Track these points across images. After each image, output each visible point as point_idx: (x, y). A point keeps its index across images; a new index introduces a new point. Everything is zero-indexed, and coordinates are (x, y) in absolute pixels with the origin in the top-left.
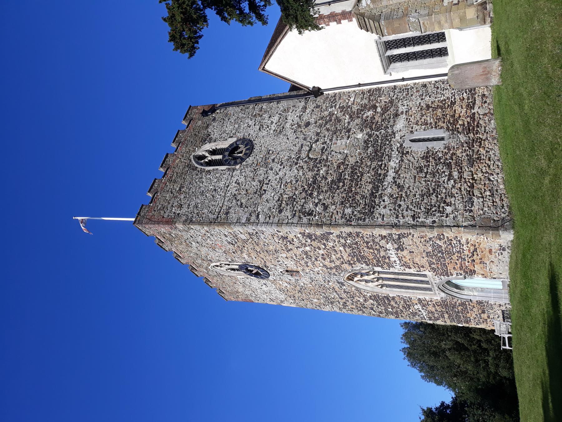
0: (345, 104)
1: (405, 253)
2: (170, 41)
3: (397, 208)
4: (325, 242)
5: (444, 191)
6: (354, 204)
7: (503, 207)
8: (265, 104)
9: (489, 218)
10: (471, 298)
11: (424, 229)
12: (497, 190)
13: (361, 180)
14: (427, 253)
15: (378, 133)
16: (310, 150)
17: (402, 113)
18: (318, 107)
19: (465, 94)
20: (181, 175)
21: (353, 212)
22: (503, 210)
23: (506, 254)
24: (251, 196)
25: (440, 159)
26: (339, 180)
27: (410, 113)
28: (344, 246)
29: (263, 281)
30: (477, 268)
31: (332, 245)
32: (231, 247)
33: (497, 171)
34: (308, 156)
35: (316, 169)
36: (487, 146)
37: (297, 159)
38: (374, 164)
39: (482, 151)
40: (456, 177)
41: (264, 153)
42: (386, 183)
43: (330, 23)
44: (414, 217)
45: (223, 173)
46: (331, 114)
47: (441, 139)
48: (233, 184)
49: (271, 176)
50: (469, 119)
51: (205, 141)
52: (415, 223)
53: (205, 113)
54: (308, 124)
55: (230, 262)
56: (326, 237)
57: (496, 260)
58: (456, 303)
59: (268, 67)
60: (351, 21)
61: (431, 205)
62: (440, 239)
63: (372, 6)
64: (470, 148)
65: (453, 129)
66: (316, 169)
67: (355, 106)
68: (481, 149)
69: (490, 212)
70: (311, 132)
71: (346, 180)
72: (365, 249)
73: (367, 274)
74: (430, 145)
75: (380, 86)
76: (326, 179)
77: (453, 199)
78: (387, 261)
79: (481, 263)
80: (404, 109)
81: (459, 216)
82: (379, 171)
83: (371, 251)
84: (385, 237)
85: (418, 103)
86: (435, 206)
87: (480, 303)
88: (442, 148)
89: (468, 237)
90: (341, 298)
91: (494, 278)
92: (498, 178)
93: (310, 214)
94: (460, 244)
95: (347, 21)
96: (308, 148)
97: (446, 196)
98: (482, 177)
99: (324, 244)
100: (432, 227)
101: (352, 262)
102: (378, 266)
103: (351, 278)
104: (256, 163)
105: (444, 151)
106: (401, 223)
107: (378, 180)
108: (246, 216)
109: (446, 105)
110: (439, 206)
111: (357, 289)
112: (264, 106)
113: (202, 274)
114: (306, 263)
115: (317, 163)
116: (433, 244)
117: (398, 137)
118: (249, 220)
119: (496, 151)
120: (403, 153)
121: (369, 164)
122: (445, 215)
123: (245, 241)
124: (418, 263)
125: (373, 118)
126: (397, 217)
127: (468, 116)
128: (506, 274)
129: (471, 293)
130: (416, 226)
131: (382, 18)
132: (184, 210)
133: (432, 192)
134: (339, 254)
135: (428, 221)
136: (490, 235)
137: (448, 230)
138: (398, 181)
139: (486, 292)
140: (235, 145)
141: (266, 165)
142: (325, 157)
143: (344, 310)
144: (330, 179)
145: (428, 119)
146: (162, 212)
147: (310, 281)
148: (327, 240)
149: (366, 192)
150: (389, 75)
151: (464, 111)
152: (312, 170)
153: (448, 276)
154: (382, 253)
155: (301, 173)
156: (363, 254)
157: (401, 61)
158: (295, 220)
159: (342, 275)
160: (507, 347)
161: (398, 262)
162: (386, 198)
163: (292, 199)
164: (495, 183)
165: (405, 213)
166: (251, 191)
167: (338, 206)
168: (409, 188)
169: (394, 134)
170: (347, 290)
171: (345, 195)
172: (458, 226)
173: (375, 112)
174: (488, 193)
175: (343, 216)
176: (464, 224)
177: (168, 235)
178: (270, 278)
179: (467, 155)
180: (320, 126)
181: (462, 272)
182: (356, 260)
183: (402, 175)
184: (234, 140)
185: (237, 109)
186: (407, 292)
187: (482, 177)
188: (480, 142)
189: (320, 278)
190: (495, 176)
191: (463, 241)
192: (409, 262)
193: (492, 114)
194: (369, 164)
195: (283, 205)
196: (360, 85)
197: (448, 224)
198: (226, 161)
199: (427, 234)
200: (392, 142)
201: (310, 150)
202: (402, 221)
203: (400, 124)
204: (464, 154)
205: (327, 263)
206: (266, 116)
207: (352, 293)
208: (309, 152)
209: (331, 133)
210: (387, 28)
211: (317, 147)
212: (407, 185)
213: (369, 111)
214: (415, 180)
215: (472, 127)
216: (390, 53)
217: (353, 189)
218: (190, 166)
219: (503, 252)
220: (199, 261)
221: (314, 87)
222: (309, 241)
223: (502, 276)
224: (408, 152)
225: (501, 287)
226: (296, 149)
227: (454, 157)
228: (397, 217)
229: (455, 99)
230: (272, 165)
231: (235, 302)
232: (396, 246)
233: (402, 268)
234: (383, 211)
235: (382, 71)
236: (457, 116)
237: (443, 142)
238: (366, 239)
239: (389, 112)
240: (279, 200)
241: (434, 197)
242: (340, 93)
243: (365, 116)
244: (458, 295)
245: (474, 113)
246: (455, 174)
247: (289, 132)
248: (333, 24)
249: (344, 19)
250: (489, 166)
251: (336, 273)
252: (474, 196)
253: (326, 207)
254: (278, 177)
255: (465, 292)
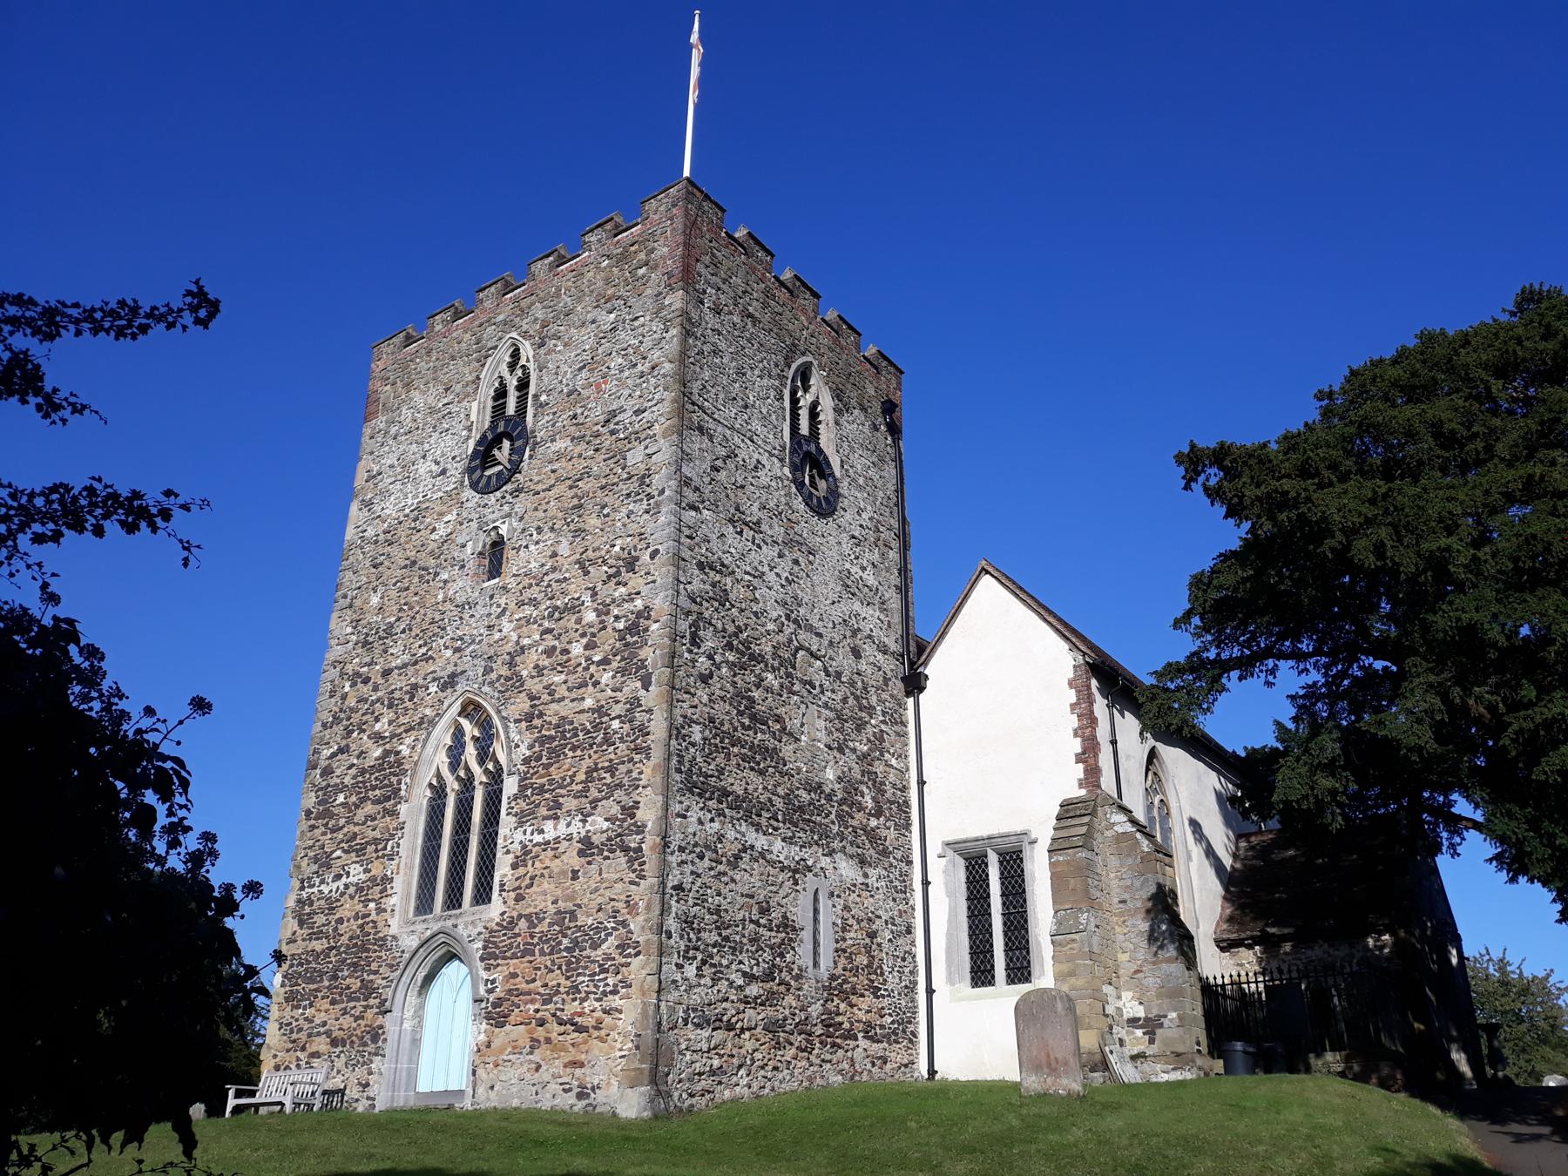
0: (886, 744)
1: (572, 859)
3: (698, 850)
4: (615, 665)
5: (725, 962)
6: (711, 749)
7: (691, 1095)
10: (396, 1013)
11: (658, 912)
12: (720, 1083)
13: (752, 769)
14: (572, 913)
15: (833, 816)
16: (812, 654)
17: (866, 876)
18: (886, 680)
19: (890, 1020)
20: (776, 327)
22: (685, 1095)
24: (732, 496)
25: (782, 955)
26: (753, 717)
27: (864, 894)
29: (456, 470)
30: (515, 1032)
31: (603, 681)
32: (598, 413)
33: (755, 1086)
34: (801, 647)
35: (776, 664)
37: (796, 621)
38: (779, 803)
40: (747, 991)
43: (1079, 740)
44: (679, 888)
46: (870, 710)
47: (816, 957)
48: (756, 456)
49: (769, 552)
50: (846, 1025)
51: (838, 396)
52: (668, 890)
53: (889, 407)
54: (856, 653)
55: (536, 397)
56: (632, 667)
57: (544, 1075)
58: (376, 972)
60: (1081, 786)
63: (1109, 833)
65: (837, 989)
66: (776, 664)
67: (882, 768)
68: (793, 1051)
69: (684, 1064)
70: (843, 661)
71: (750, 732)
72: (587, 763)
74: (806, 935)
75: (915, 828)
76: (758, 686)
78: (543, 811)
79: (533, 1040)
81: (677, 994)
83: (581, 777)
84: (632, 816)
85: (880, 912)
86: (699, 939)
87: (376, 1034)
88: (800, 962)
89: (629, 1013)
90: (386, 673)
92: (741, 1087)
93: (695, 641)
94: (605, 994)
95: (1082, 776)
96: (814, 648)
97: (713, 965)
98: (743, 1051)
99: (605, 661)
100: (660, 928)
101: (537, 722)
104: (793, 517)
106: (670, 858)
108: (695, 478)
109: (873, 977)
110: (697, 949)
111: (428, 724)
113: (488, 304)
114: (534, 602)
115: (787, 666)
116: (606, 928)
117: (825, 862)
118: (687, 484)
119: (787, 1083)
120: (796, 871)
121: (781, 791)
123: (618, 457)
124: (534, 888)
125: (861, 809)
126: (682, 849)
127: (852, 1024)
128: (488, 1100)
129: (408, 1014)
130: (664, 894)
132: (711, 320)
133: (724, 933)
134: (566, 694)
135: (671, 921)
138: (746, 857)
140: (827, 471)
141: (790, 543)
142: (796, 688)
144: (756, 694)
147: (460, 600)
148: (622, 671)
149: (731, 780)
151: (861, 1015)
153: (482, 959)
154: (570, 803)
155: (771, 626)
156: (570, 754)
157: (969, 882)
158: (684, 602)
159: (486, 689)
160: (232, 1102)
161: (538, 838)
162: (716, 825)
163: (723, 599)
164: (735, 1079)
165: (688, 868)
167: (707, 709)
168: (733, 880)
172: (659, 992)
173: (870, 814)
174: (716, 1063)
176: (663, 1004)
177: (642, 256)
178: (468, 493)
179: (785, 1019)
180: (852, 684)
183: (756, 866)
185: (891, 487)
187: (743, 1051)
189: (473, 627)
190: (745, 1081)
191: (616, 1001)
192: (537, 864)
195: (712, 574)
197: (664, 968)
198: (799, 443)
199: (641, 918)
200: (815, 847)
201: (812, 654)
203: (848, 870)
205: (533, 657)
208: (808, 650)
210: (1068, 862)
212: (737, 877)
213: (873, 799)
215: (834, 1032)
217: (736, 750)
220: (539, 312)
222: (621, 625)
224: (796, 883)
225: (423, 1087)
227: (782, 989)
228: (682, 849)
230: (789, 557)
231: (369, 371)
234: (693, 817)
235: (951, 838)
236: (854, 999)
237: (811, 964)
238: (623, 768)
239: (868, 846)
240: (723, 565)
242: (905, 735)
246: (753, 990)
247: (843, 609)
248: (1077, 745)
249: (1086, 771)
250: (762, 1068)
252: (714, 1029)
253: (705, 679)
254: (766, 569)
255: (412, 999)
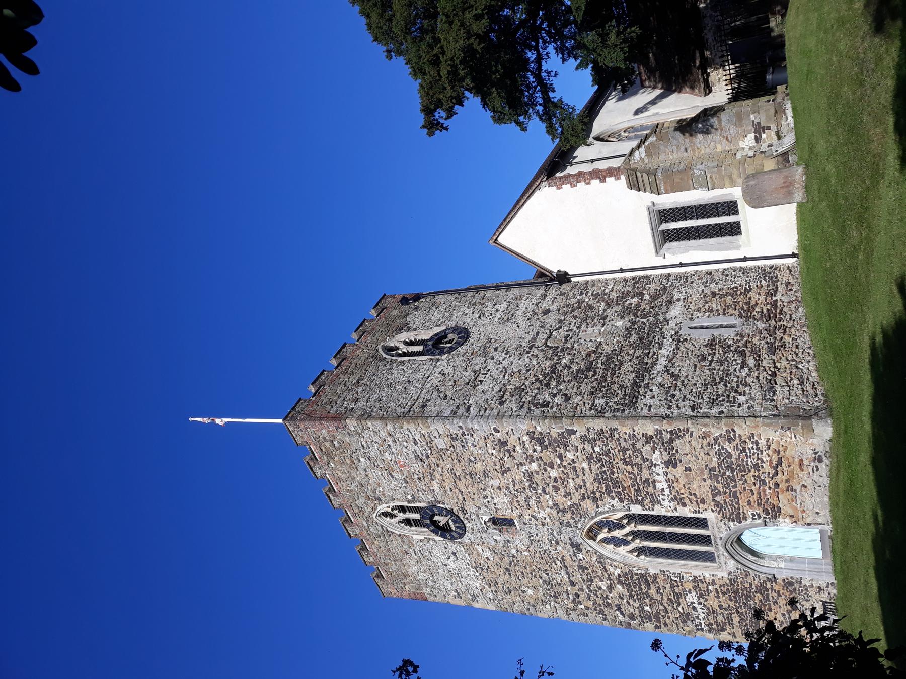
1: (679, 471)
2: (424, 127)
3: (669, 398)
4: (562, 451)
5: (735, 379)
6: (609, 394)
7: (816, 395)
8: (489, 292)
10: (775, 572)
11: (708, 420)
12: (808, 379)
13: (619, 369)
14: (711, 470)
15: (645, 321)
16: (549, 337)
17: (679, 300)
18: (562, 294)
19: (763, 282)
22: (817, 399)
23: (824, 468)
24: (460, 387)
25: (729, 346)
26: (589, 369)
27: (689, 300)
28: (589, 459)
29: (452, 547)
30: (783, 501)
33: (808, 358)
34: (546, 344)
35: (556, 358)
36: (794, 333)
37: (530, 348)
39: (787, 338)
40: (752, 365)
41: (483, 339)
44: (693, 408)
45: (423, 363)
46: (580, 302)
48: (437, 375)
49: (491, 364)
50: (769, 307)
52: (695, 414)
53: (405, 301)
54: (547, 312)
55: (409, 502)
57: (808, 483)
58: (751, 584)
60: (619, 178)
61: (718, 395)
62: (730, 440)
63: (646, 161)
64: (770, 336)
65: (747, 313)
66: (556, 358)
67: (614, 294)
69: (798, 400)
71: (599, 371)
72: (621, 465)
73: (619, 525)
74: (716, 333)
75: (648, 272)
76: (570, 368)
77: (748, 388)
78: (651, 489)
81: (756, 407)
82: (646, 360)
83: (629, 468)
84: (651, 437)
85: (700, 290)
86: (723, 395)
87: (788, 584)
90: (572, 584)
92: (810, 367)
93: (546, 405)
94: (758, 449)
95: (613, 178)
96: (545, 336)
98: (788, 366)
99: (560, 456)
101: (598, 495)
102: (637, 502)
103: (592, 534)
104: (470, 352)
105: (736, 338)
106: (675, 414)
109: (739, 292)
111: (601, 559)
112: (489, 294)
114: (527, 499)
116: (719, 450)
117: (672, 324)
118: (455, 413)
120: (679, 341)
121: (631, 352)
122: (737, 405)
123: (441, 453)
126: (670, 408)
129: (775, 565)
132: (362, 403)
134: (580, 478)
135: (713, 412)
136: (800, 428)
137: (740, 421)
141: (485, 353)
142: (569, 346)
143: (574, 615)
146: (328, 407)
148: (566, 446)
149: (627, 381)
150: (661, 258)
151: (762, 298)
153: (740, 522)
154: (645, 474)
155: (534, 362)
156: (616, 475)
157: (679, 240)
158: (523, 412)
159: (579, 526)
161: (667, 492)
162: (654, 388)
163: (520, 390)
164: (805, 370)
165: (681, 403)
166: (462, 381)
167: (586, 397)
168: (686, 377)
169: (667, 321)
171: (596, 386)
173: (642, 299)
174: (796, 382)
176: (763, 414)
177: (328, 444)
178: (466, 539)
179: (767, 343)
180: (565, 313)
182: (604, 490)
183: (677, 364)
184: (443, 328)
185: (450, 297)
186: (676, 565)
188: (785, 331)
189: (543, 534)
191: (762, 442)
192: (682, 492)
193: (800, 302)
195: (506, 397)
196: (621, 270)
197: (741, 414)
199: (712, 430)
201: (549, 337)
203: (676, 311)
204: (763, 342)
205: (559, 499)
206: (490, 304)
207: (590, 570)
210: (665, 183)
212: (685, 374)
213: (632, 298)
214: (695, 368)
215: (773, 313)
216: (665, 227)
217: (608, 379)
218: (376, 357)
219: (819, 465)
220: (361, 502)
221: (559, 271)
222: (539, 448)
223: (820, 520)
224: (686, 340)
227: (749, 345)
228: (670, 408)
229: (750, 286)
232: (666, 458)
233: (672, 504)
234: (649, 402)
235: (653, 251)
236: (752, 303)
237: (733, 329)
238: (623, 444)
239: (661, 300)
240: (500, 391)
241: (721, 387)
242: (593, 282)
243: (628, 302)
244: (754, 567)
245: (776, 301)
246: (751, 362)
248: (595, 182)
249: (610, 176)
251: (571, 521)
254: (501, 366)
255: (766, 562)
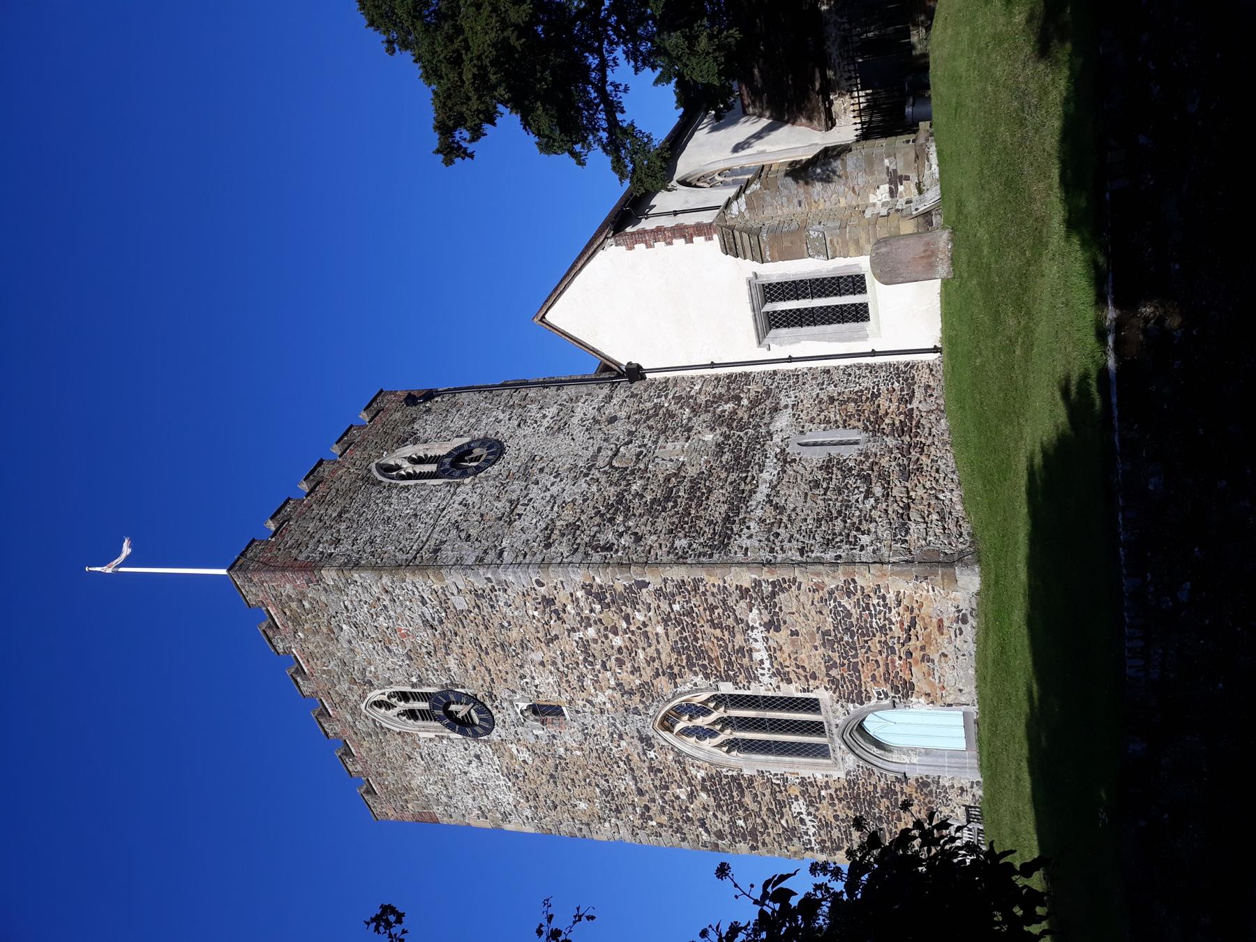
1: (783, 636)
4: (629, 610)
5: (857, 513)
7: (961, 535)
9: (939, 552)
10: (906, 769)
11: (821, 567)
12: (950, 513)
13: (707, 498)
16: (615, 455)
17: (786, 407)
19: (896, 384)
20: (350, 493)
21: (690, 545)
22: (961, 540)
23: (969, 631)
24: (489, 524)
25: (850, 469)
26: (667, 499)
27: (800, 407)
29: (475, 747)
33: (950, 486)
35: (624, 483)
37: (589, 469)
42: (754, 503)
43: (674, 241)
46: (657, 407)
48: (456, 506)
49: (534, 492)
53: (411, 400)
54: (612, 420)
55: (413, 686)
56: (630, 597)
58: (875, 787)
59: (554, 316)
60: (711, 239)
63: (747, 216)
65: (874, 425)
66: (624, 483)
67: (703, 397)
69: (937, 541)
72: (707, 628)
74: (834, 451)
76: (642, 496)
77: (874, 524)
78: (746, 661)
79: (923, 660)
80: (790, 402)
83: (718, 632)
85: (814, 394)
86: (841, 534)
89: (900, 586)
90: (641, 793)
91: (950, 705)
92: (953, 497)
93: (608, 547)
94: (885, 606)
96: (610, 453)
98: (925, 496)
99: (627, 618)
101: (676, 670)
102: (728, 678)
106: (779, 560)
107: (738, 501)
110: (848, 535)
111: (680, 757)
112: (532, 393)
113: (338, 729)
114: (581, 678)
116: (835, 607)
118: (482, 560)
120: (785, 461)
121: (723, 476)
123: (461, 617)
125: (734, 412)
128: (970, 693)
131: (764, 231)
132: (345, 546)
134: (653, 648)
136: (939, 578)
138: (776, 500)
139: (935, 756)
141: (526, 476)
142: (642, 466)
144: (649, 498)
145: (832, 415)
148: (634, 604)
149: (717, 515)
150: (765, 349)
151: (894, 406)
152: (617, 484)
153: (862, 703)
154: (739, 640)
155: (594, 488)
156: (700, 642)
158: (578, 557)
159: (651, 712)
161: (767, 664)
162: (752, 524)
163: (574, 527)
165: (787, 545)
166: (492, 515)
168: (794, 510)
170: (655, 764)
171: (677, 521)
172: (882, 563)
173: (739, 405)
175: (672, 549)
176: (892, 560)
177: (294, 605)
178: (494, 736)
179: (899, 465)
180: (637, 422)
181: (887, 688)
187: (925, 496)
191: (891, 597)
192: (787, 663)
194: (723, 476)
195: (554, 537)
196: (713, 365)
198: (444, 471)
199: (827, 580)
201: (615, 455)
202: (780, 557)
203: (782, 421)
205: (625, 676)
206: (534, 407)
209: (656, 432)
210: (771, 247)
211: (628, 452)
212: (792, 506)
215: (908, 426)
216: (770, 307)
217: (693, 512)
221: (630, 363)
222: (598, 607)
223: (963, 700)
224: (794, 460)
226: (590, 453)
227: (876, 468)
234: (746, 543)
235: (755, 340)
236: (882, 412)
238: (711, 600)
239: (763, 406)
240: (546, 529)
241: (839, 522)
242: (675, 379)
243: (721, 409)
246: (878, 490)
248: (679, 243)
253: (638, 538)
254: (548, 494)
255: (894, 757)
